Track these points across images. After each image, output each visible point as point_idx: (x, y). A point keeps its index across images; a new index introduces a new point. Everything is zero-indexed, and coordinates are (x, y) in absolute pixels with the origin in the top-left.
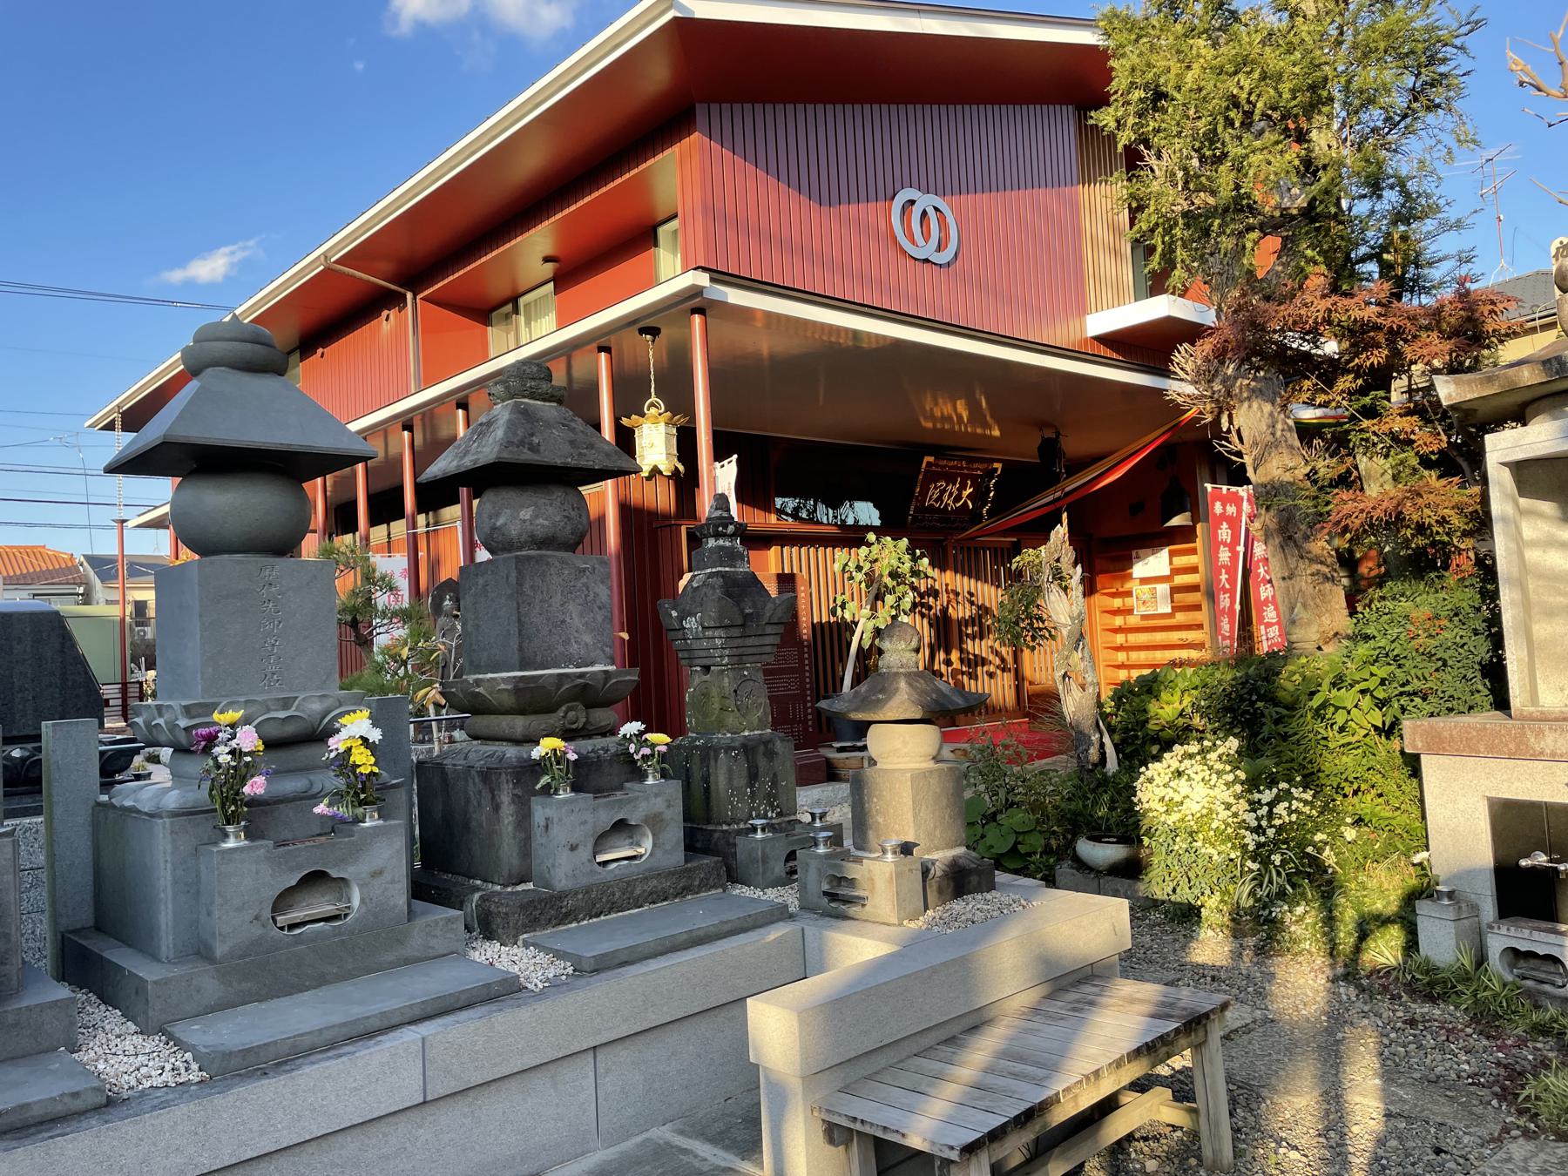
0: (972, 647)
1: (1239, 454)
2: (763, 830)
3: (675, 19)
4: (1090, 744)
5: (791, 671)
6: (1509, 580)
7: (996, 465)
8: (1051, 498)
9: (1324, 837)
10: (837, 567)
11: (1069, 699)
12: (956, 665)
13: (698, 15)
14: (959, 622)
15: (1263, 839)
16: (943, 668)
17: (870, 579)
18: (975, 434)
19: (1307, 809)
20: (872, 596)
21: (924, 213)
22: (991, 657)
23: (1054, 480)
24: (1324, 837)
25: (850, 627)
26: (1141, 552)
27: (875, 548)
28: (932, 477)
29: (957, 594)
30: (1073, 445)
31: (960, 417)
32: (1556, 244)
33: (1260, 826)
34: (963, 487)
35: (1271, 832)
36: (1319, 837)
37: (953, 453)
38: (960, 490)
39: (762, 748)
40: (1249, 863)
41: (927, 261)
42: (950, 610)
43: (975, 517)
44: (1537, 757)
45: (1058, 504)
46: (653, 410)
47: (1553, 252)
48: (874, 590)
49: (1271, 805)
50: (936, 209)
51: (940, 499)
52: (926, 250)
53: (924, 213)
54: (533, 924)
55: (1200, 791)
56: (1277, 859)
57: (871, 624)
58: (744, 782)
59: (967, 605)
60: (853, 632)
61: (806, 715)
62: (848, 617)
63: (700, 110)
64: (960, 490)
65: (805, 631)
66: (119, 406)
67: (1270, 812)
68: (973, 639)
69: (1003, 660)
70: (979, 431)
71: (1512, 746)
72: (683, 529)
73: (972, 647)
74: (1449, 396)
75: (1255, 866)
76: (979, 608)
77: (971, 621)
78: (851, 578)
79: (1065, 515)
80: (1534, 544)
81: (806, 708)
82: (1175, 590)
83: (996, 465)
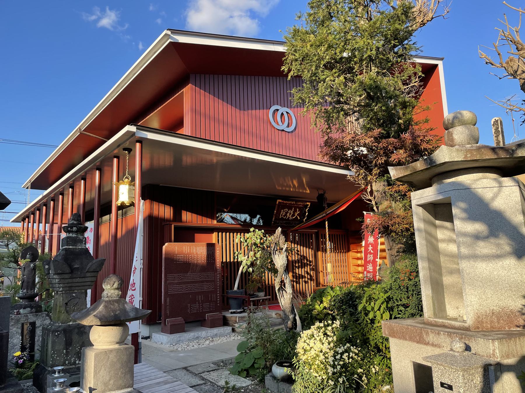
1: (370, 201)
2: (59, 372)
3: (170, 42)
4: (289, 319)
5: (211, 281)
6: (422, 258)
7: (308, 203)
8: (321, 216)
9: (362, 371)
11: (282, 300)
13: (180, 41)
15: (335, 370)
18: (299, 192)
19: (356, 357)
21: (282, 114)
23: (323, 209)
24: (362, 371)
25: (239, 264)
28: (282, 206)
30: (329, 196)
31: (294, 186)
32: (493, 120)
33: (334, 364)
34: (295, 211)
35: (339, 367)
36: (360, 370)
37: (291, 200)
39: (76, 330)
40: (330, 381)
41: (283, 130)
43: (301, 221)
44: (427, 344)
46: (126, 180)
47: (492, 123)
49: (342, 354)
50: (287, 113)
51: (286, 215)
52: (284, 127)
53: (282, 114)
55: (319, 345)
56: (341, 380)
58: (61, 347)
59: (296, 255)
61: (217, 298)
63: (192, 77)
65: (218, 264)
66: (30, 181)
67: (341, 357)
69: (311, 276)
70: (301, 191)
71: (418, 338)
72: (173, 226)
74: (394, 175)
75: (332, 383)
79: (327, 222)
80: (443, 241)
81: (216, 296)
83: (308, 203)
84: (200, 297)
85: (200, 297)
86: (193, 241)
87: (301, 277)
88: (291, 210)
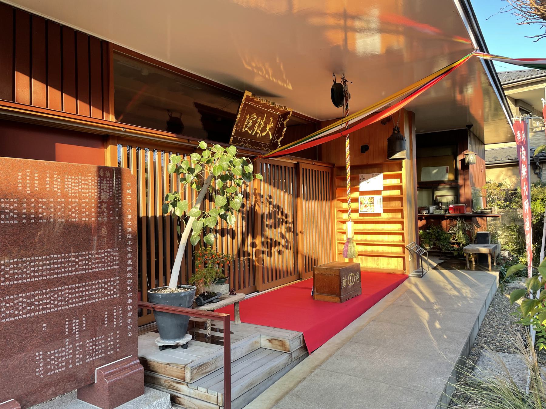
0: (273, 234)
5: (111, 274)
10: (171, 167)
14: (262, 217)
16: (250, 249)
17: (200, 181)
20: (202, 196)
22: (280, 240)
26: (365, 175)
27: (207, 154)
29: (262, 196)
38: (266, 124)
42: (257, 208)
45: (344, 133)
48: (204, 191)
51: (252, 128)
57: (200, 224)
62: (178, 213)
64: (266, 124)
69: (287, 241)
73: (273, 234)
76: (275, 206)
77: (270, 216)
78: (184, 179)
79: (348, 142)
82: (385, 199)
84: (75, 323)
85: (76, 322)
86: (51, 156)
87: (226, 232)
88: (262, 118)
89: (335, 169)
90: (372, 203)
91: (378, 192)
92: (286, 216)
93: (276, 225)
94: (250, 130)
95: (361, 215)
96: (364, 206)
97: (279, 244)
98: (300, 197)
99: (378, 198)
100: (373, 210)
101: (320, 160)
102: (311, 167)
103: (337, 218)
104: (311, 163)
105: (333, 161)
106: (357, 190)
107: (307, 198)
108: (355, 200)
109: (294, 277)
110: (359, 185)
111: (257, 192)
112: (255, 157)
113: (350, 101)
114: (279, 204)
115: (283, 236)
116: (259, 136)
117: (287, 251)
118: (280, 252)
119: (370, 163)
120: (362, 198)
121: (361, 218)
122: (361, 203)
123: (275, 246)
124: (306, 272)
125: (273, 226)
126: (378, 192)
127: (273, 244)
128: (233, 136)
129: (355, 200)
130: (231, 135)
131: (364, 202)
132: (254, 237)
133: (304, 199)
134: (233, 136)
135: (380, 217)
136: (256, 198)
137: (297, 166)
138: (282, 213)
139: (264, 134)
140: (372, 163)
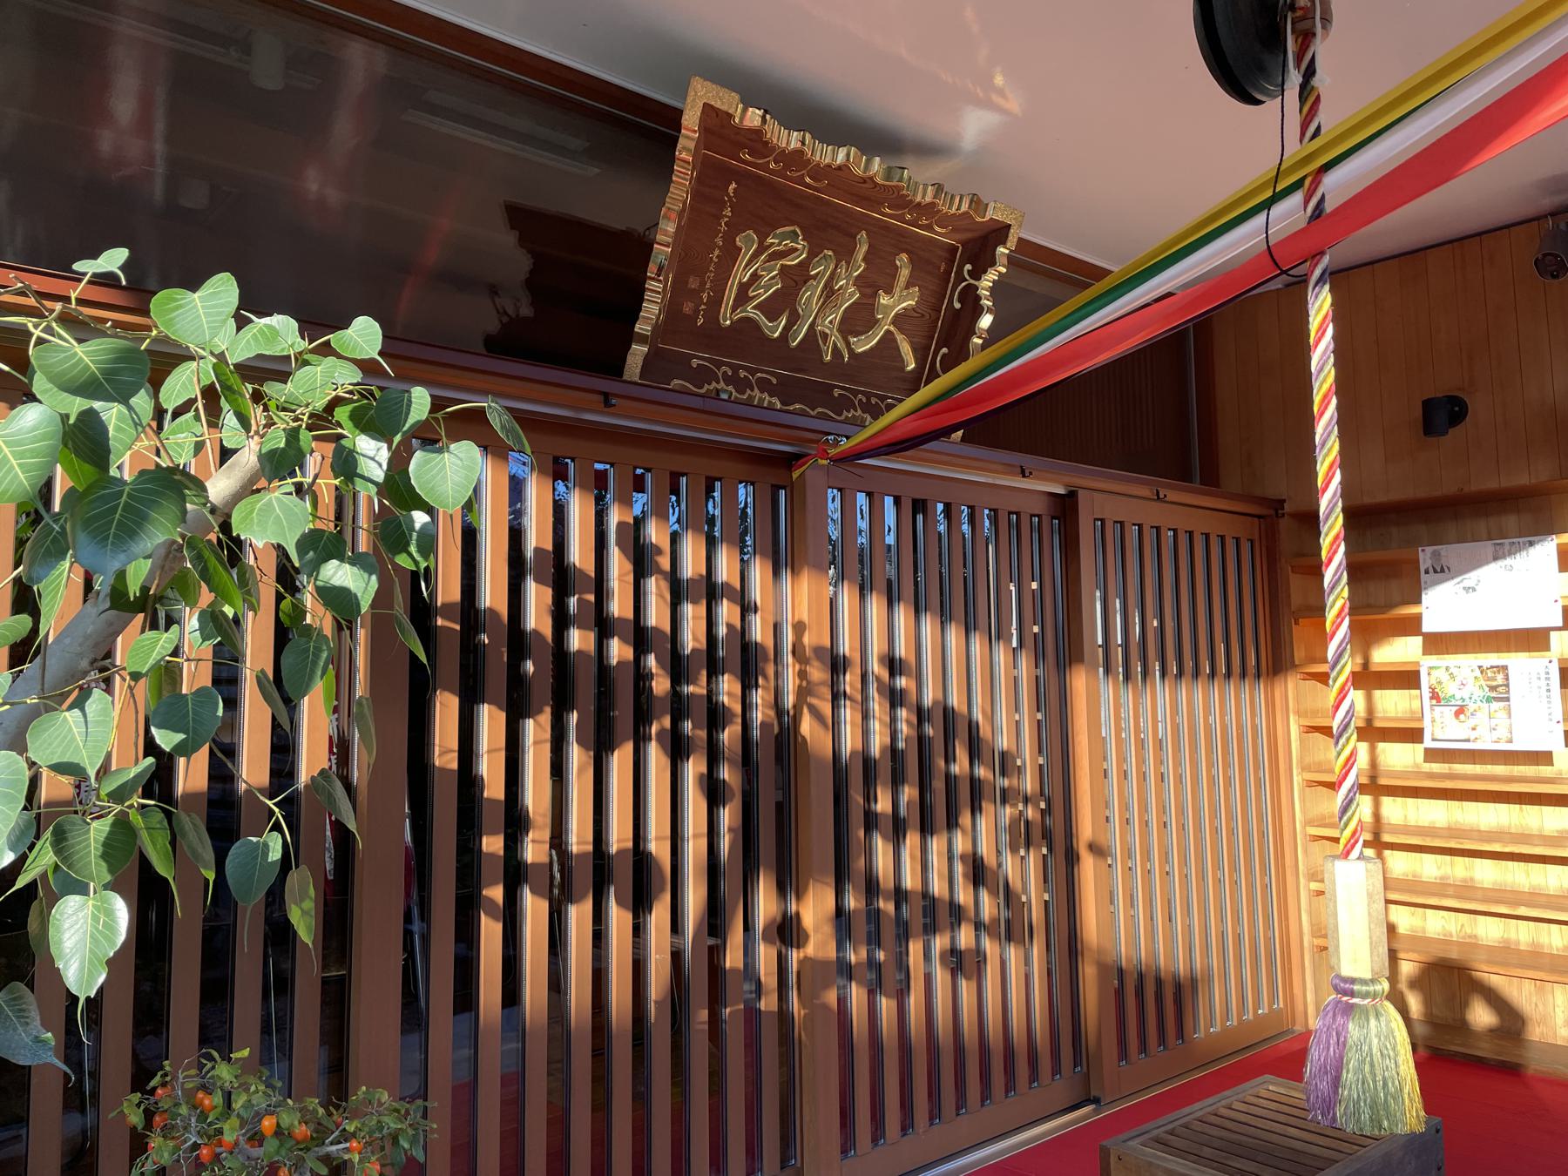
0: (914, 864)
12: (819, 943)
29: (837, 665)
38: (872, 285)
54: (710, 925)
60: (756, 141)
64: (872, 285)
68: (897, 830)
69: (1009, 896)
73: (914, 864)
79: (1321, 305)
88: (845, 254)
89: (1284, 524)
90: (1499, 692)
91: (1533, 640)
92: (1006, 764)
93: (941, 808)
94: (773, 317)
95: (1432, 755)
96: (1449, 712)
97: (956, 913)
98: (1080, 660)
99: (1531, 674)
100: (1502, 733)
101: (1211, 479)
102: (1153, 514)
103: (1304, 769)
104: (1145, 491)
105: (1276, 487)
106: (1411, 626)
107: (1136, 663)
108: (1407, 678)
109: (1059, 1088)
110: (1418, 601)
111: (806, 640)
112: (797, 457)
113: (1322, 49)
114: (955, 700)
115: (978, 873)
116: (837, 352)
117: (1013, 954)
118: (961, 963)
119: (1475, 486)
120: (1436, 669)
121: (1436, 767)
122: (1435, 696)
123: (931, 929)
124: (1123, 1054)
125: (915, 819)
126: (1533, 640)
127: (917, 921)
128: (642, 339)
129: (1407, 678)
130: (629, 337)
131: (1449, 689)
132: (786, 884)
133: (1107, 671)
134: (642, 339)
135: (1544, 771)
136: (802, 675)
137: (1065, 507)
138: (976, 749)
139: (864, 345)
140: (1492, 484)
